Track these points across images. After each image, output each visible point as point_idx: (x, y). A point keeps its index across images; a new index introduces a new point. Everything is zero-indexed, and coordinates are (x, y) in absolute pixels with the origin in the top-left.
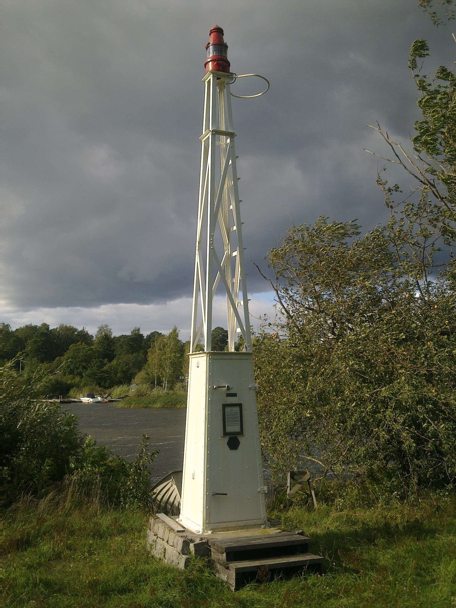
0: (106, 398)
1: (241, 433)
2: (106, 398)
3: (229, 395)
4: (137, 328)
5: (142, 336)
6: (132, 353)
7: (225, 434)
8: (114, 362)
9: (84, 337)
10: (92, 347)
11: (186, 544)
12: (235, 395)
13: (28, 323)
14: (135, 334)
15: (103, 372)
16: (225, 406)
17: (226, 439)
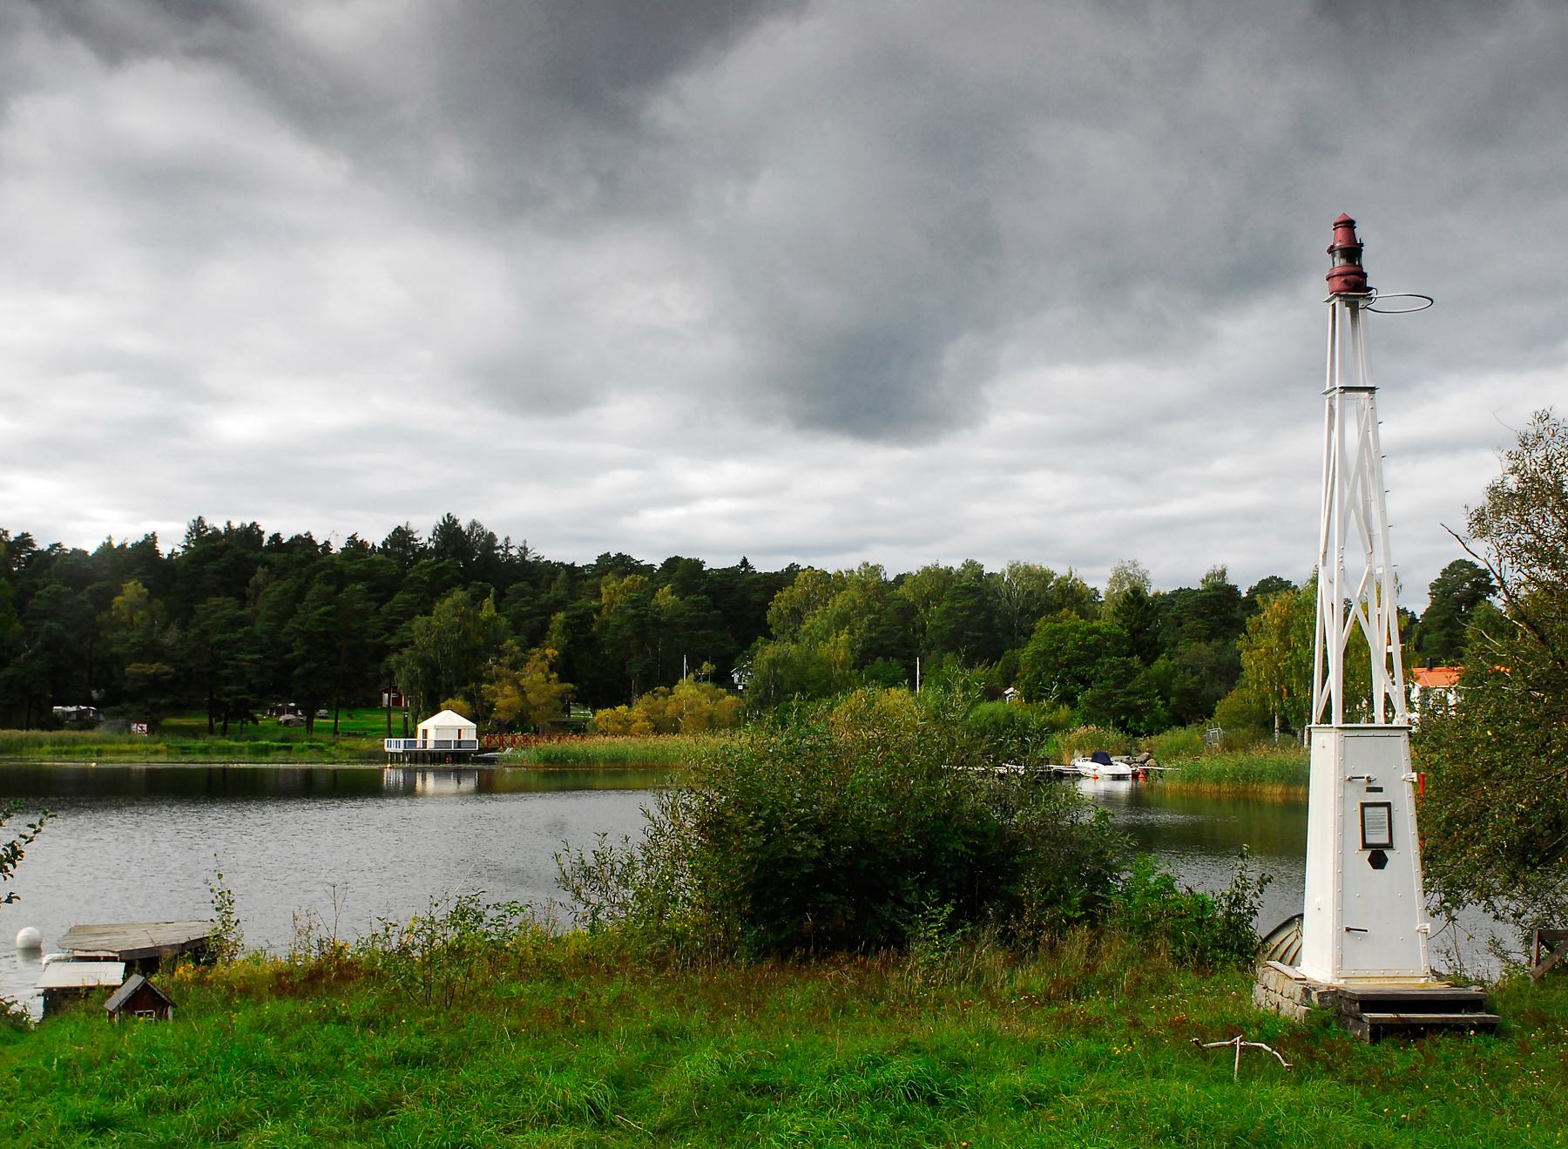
0: (1143, 763)
1: (1390, 846)
2: (1143, 763)
3: (1370, 790)
4: (1219, 568)
5: (1233, 590)
6: (1208, 639)
7: (1365, 846)
8: (1161, 664)
9: (1073, 597)
10: (1095, 624)
11: (1307, 992)
12: (1380, 790)
13: (929, 563)
14: (1215, 587)
15: (1129, 694)
16: (1364, 806)
17: (1368, 853)
